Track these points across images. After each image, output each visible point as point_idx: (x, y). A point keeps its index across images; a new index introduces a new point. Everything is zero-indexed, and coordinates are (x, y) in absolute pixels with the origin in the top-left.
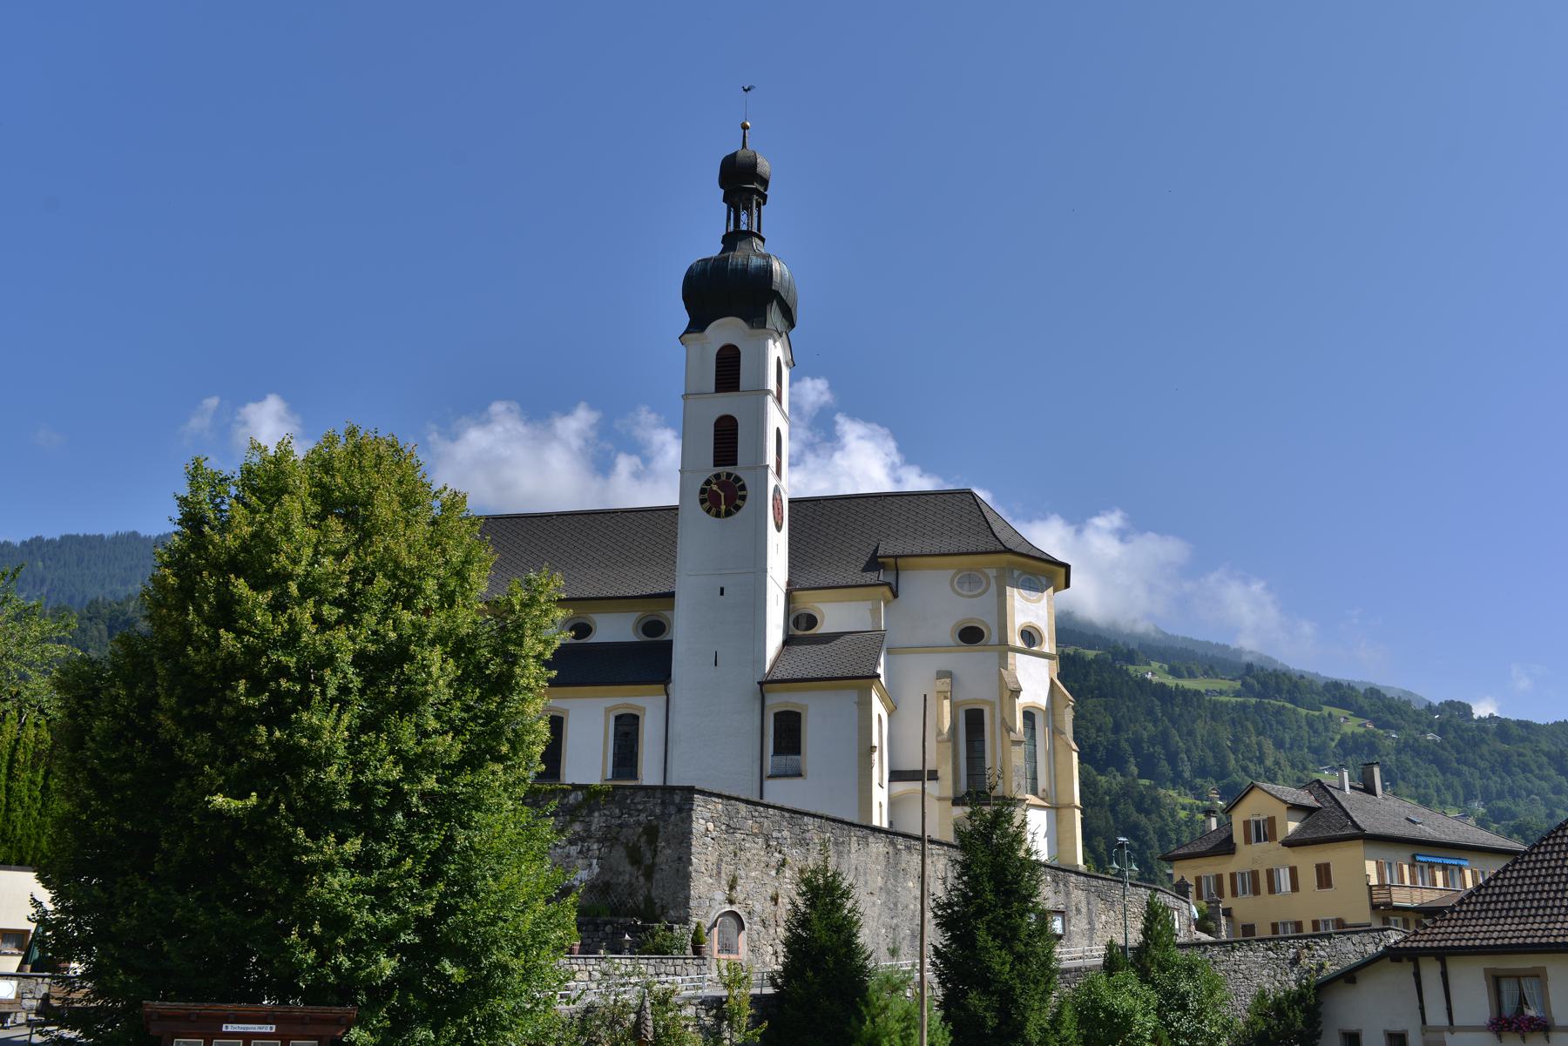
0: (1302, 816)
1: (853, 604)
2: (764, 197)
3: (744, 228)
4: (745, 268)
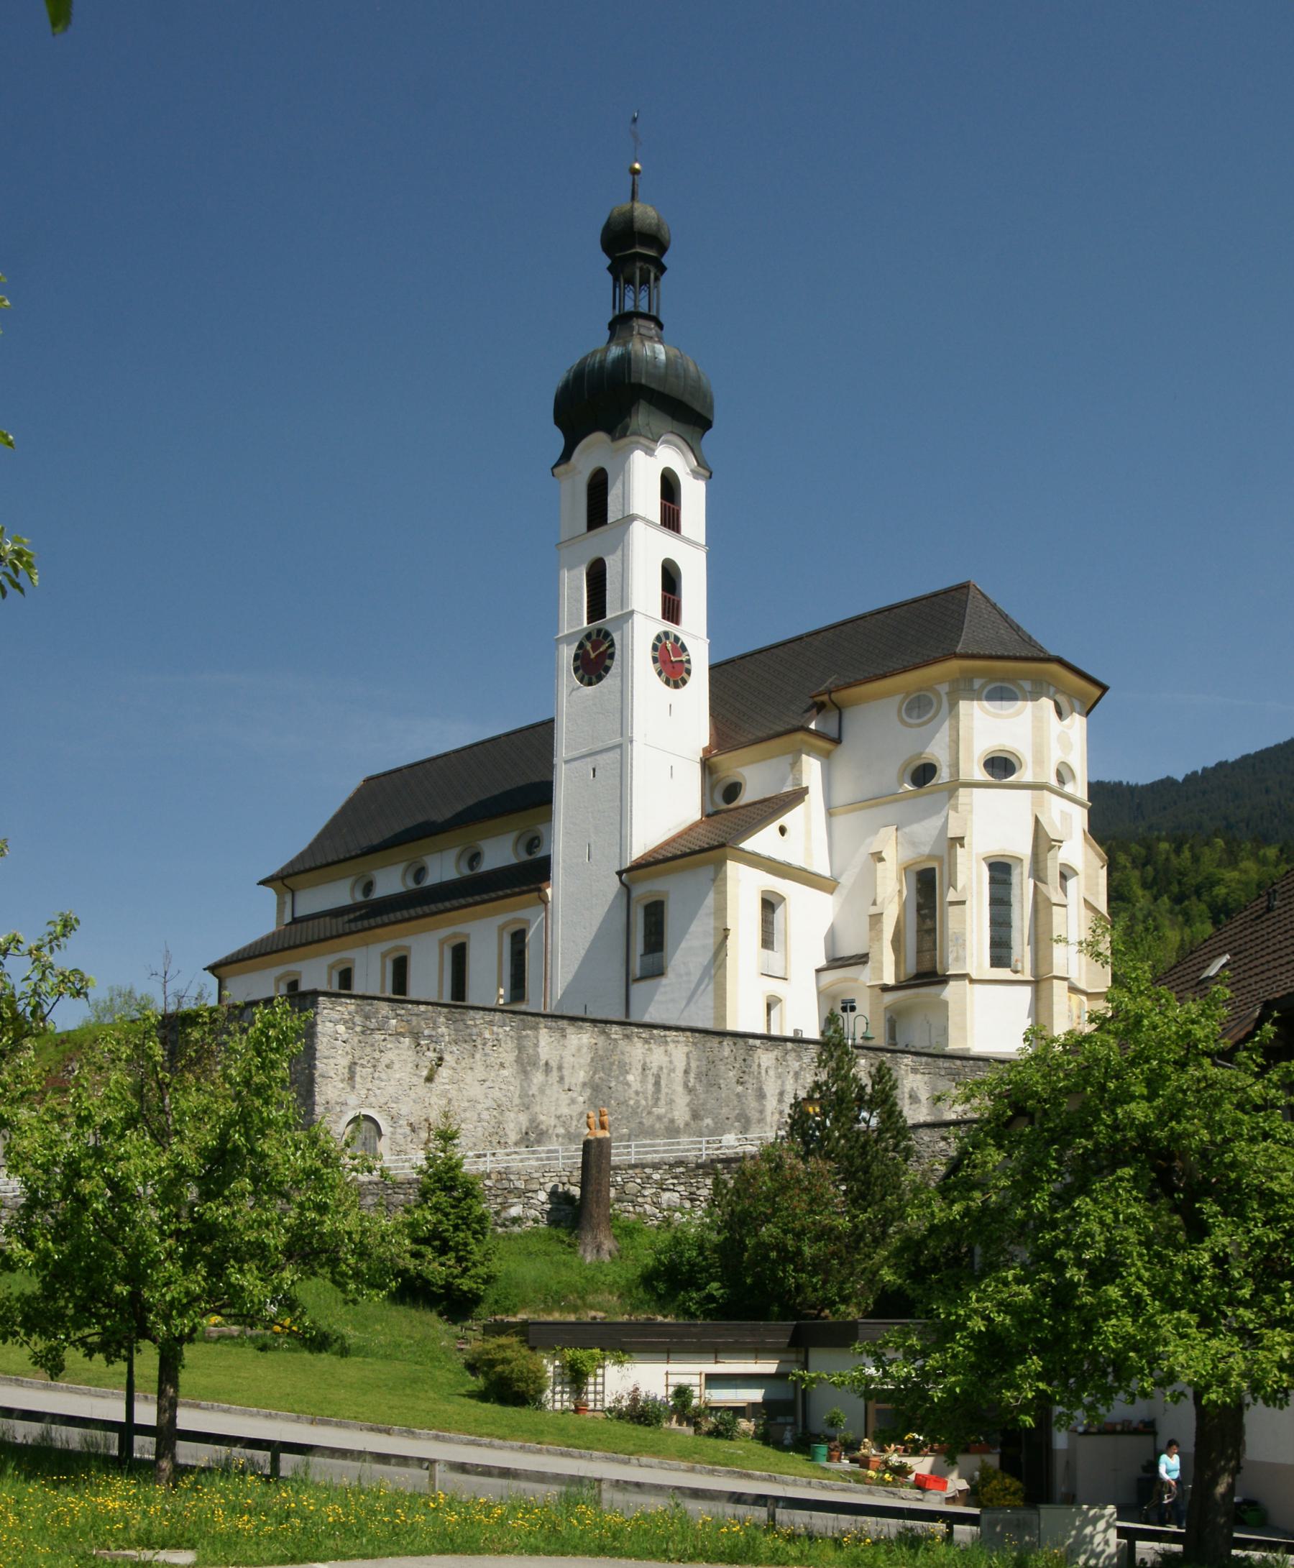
1: (774, 761)
2: (662, 269)
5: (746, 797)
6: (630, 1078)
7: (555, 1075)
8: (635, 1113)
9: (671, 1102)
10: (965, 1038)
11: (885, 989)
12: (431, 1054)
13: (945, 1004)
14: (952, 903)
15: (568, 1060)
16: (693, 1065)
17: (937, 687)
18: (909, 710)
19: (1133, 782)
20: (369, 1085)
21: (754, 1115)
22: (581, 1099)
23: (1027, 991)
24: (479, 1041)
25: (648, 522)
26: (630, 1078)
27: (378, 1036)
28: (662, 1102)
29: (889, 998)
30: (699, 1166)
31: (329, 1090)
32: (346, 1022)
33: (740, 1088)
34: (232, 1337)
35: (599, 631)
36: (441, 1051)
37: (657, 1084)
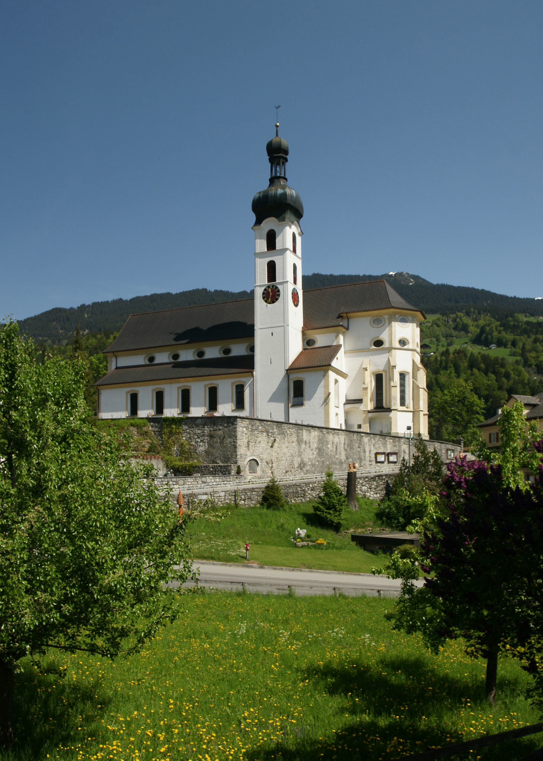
0: (530, 408)
2: (287, 161)
3: (278, 175)
4: (276, 194)
5: (317, 345)
6: (329, 446)
7: (308, 445)
8: (330, 457)
9: (340, 454)
10: (397, 429)
11: (369, 412)
12: (272, 438)
13: (390, 418)
14: (393, 387)
15: (312, 440)
16: (346, 442)
17: (384, 316)
18: (374, 322)
19: (233, 291)
20: (254, 449)
21: (363, 458)
22: (315, 453)
23: (411, 414)
24: (286, 434)
25: (290, 251)
26: (329, 446)
27: (256, 432)
28: (338, 454)
29: (370, 415)
30: (372, 478)
31: (241, 450)
32: (246, 427)
33: (359, 449)
34: (305, 546)
35: (273, 286)
36: (275, 437)
37: (336, 448)
